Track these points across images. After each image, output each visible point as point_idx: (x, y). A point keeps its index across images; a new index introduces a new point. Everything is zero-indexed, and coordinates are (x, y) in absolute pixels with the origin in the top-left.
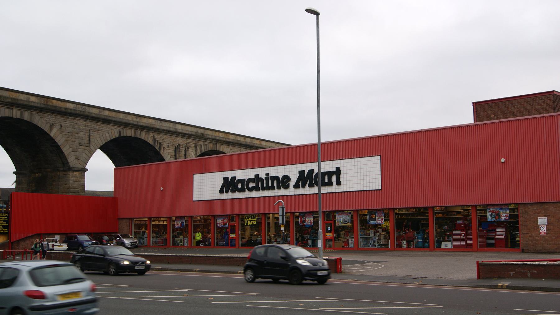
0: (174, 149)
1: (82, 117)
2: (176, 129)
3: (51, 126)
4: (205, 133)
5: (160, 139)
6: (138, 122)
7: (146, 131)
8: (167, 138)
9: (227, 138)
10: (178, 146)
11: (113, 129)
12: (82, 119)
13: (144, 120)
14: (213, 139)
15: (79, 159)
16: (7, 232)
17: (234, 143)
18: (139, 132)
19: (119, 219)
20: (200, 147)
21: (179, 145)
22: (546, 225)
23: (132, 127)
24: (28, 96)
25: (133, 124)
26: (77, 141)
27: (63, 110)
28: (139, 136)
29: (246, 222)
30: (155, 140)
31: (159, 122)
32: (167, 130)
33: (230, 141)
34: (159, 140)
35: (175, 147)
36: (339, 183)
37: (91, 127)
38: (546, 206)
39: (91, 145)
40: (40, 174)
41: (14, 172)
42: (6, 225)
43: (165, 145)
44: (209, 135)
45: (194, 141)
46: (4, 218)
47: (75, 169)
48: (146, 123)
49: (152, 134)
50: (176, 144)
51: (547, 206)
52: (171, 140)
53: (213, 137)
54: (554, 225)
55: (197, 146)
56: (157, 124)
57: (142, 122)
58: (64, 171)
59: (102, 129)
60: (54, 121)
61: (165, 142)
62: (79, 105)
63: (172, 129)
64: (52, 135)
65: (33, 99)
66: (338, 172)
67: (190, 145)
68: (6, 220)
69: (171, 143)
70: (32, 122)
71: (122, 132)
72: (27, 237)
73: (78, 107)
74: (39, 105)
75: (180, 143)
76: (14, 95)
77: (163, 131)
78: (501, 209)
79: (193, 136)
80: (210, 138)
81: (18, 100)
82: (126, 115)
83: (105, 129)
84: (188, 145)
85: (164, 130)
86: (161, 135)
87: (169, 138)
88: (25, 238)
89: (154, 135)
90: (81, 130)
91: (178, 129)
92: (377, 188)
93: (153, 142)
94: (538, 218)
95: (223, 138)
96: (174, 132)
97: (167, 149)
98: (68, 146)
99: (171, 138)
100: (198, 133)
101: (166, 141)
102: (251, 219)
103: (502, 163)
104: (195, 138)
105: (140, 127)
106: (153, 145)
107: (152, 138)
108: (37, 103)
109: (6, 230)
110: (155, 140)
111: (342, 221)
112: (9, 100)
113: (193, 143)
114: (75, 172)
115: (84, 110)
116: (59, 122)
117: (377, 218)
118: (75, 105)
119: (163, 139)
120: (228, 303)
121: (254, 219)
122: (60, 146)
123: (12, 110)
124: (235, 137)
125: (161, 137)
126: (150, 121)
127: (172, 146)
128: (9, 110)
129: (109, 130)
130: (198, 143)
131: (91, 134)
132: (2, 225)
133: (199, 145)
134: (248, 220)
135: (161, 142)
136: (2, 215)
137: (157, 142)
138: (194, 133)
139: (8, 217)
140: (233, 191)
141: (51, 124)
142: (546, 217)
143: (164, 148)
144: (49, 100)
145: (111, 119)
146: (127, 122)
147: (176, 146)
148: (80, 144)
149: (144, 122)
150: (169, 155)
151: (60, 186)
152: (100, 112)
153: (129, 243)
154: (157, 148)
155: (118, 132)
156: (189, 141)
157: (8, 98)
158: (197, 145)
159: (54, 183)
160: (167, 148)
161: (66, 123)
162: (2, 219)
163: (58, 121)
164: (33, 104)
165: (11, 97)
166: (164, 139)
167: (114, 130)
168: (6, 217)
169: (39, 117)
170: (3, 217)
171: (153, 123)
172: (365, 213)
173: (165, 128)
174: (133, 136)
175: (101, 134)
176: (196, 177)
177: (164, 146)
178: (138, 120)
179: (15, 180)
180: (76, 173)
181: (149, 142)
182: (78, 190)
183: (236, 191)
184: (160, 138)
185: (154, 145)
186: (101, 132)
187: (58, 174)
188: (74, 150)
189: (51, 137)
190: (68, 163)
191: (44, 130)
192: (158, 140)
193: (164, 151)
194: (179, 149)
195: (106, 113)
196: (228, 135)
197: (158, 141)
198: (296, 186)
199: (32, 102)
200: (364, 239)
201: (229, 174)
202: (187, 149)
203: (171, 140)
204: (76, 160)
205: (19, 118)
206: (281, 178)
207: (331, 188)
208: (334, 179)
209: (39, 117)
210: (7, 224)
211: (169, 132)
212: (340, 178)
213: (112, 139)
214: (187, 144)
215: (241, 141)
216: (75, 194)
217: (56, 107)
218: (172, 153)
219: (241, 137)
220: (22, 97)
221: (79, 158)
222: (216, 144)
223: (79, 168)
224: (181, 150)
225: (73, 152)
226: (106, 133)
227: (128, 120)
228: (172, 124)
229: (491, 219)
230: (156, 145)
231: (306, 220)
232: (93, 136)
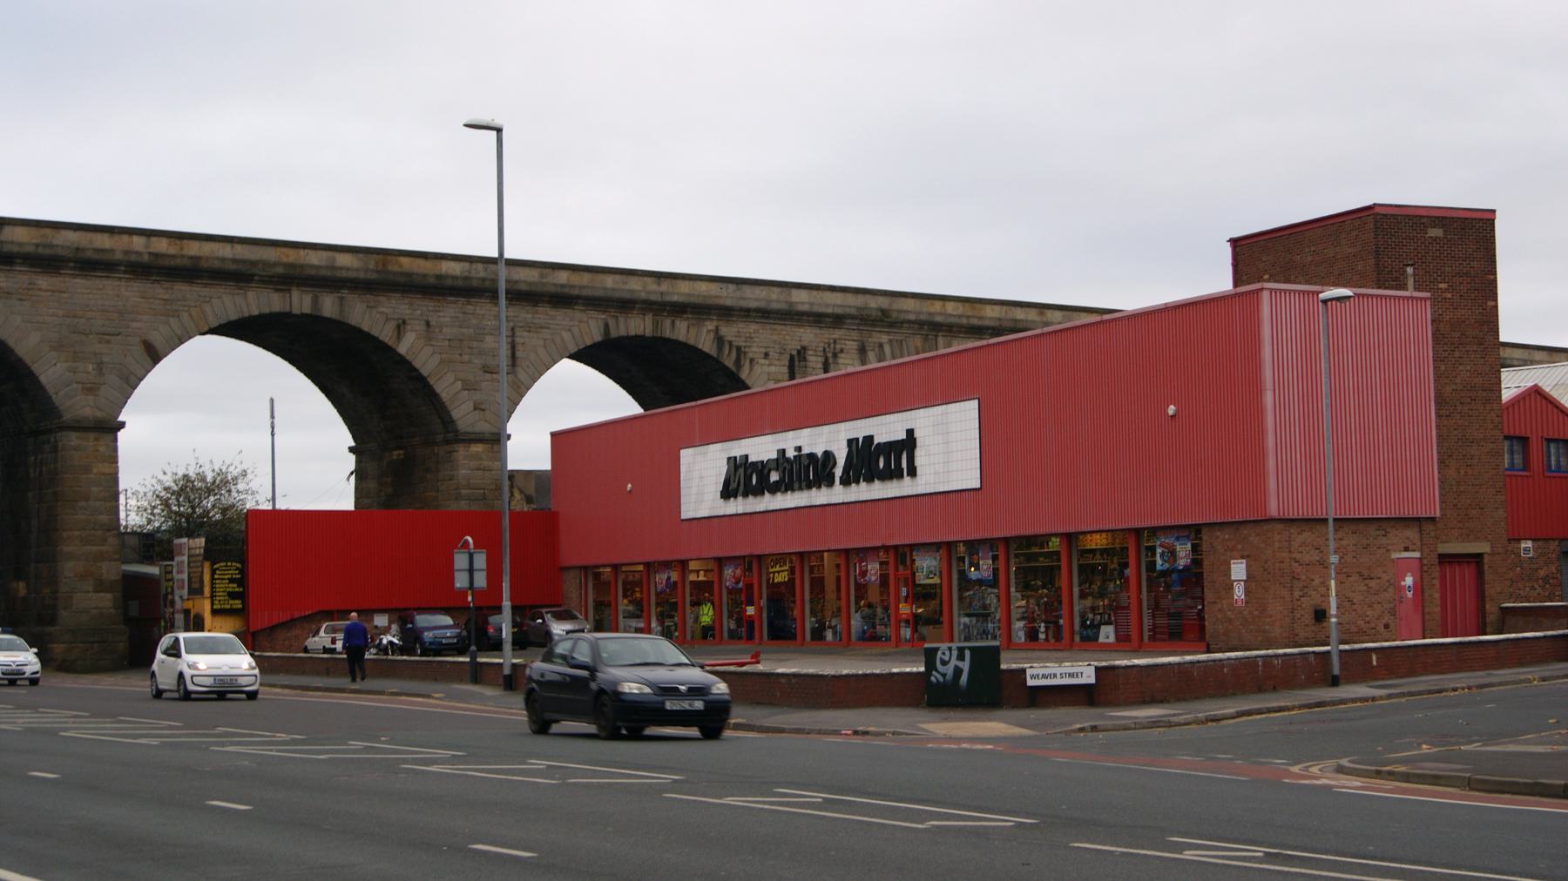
0: (787, 363)
1: (487, 294)
2: (791, 304)
3: (398, 327)
4: (895, 307)
5: (739, 337)
6: (662, 294)
7: (690, 316)
8: (761, 331)
9: (974, 317)
10: (799, 352)
11: (585, 319)
12: (488, 301)
13: (684, 287)
14: (921, 324)
15: (484, 410)
16: (239, 609)
17: (999, 330)
18: (668, 322)
19: (561, 568)
20: (877, 349)
21: (804, 348)
22: (1245, 581)
23: (642, 309)
24: (330, 254)
25: (646, 302)
26: (476, 361)
27: (432, 281)
28: (668, 331)
29: (771, 575)
30: (720, 340)
31: (732, 287)
32: (758, 310)
33: (986, 323)
34: (734, 339)
35: (791, 355)
36: (913, 472)
37: (517, 319)
38: (1245, 531)
39: (519, 370)
40: (402, 452)
41: (349, 448)
42: (237, 590)
43: (755, 351)
44: (907, 312)
45: (855, 335)
46: (232, 574)
47: (472, 437)
48: (689, 295)
49: (710, 325)
50: (793, 346)
51: (1245, 532)
52: (775, 337)
53: (923, 317)
54: (1257, 581)
55: (868, 348)
56: (726, 294)
57: (678, 294)
58: (447, 442)
59: (550, 322)
60: (408, 312)
61: (755, 344)
62: (477, 262)
63: (775, 306)
64: (402, 349)
65: (344, 260)
66: (909, 442)
67: (843, 346)
68: (235, 578)
69: (777, 346)
70: (346, 321)
71: (611, 323)
72: (292, 620)
73: (476, 269)
74: (362, 275)
75: (805, 343)
76: (291, 256)
77: (746, 314)
78: (1178, 539)
79: (848, 321)
80: (910, 322)
81: (302, 266)
82: (624, 277)
83: (559, 322)
84: (835, 349)
85: (748, 310)
86: (741, 325)
87: (770, 332)
88: (287, 622)
89: (717, 328)
90: (486, 332)
91: (797, 303)
92: (974, 487)
93: (715, 345)
94: (1232, 561)
95: (960, 316)
96: (782, 314)
97: (762, 365)
98: (450, 377)
99: (775, 330)
100: (871, 309)
101: (756, 340)
102: (780, 566)
103: (1172, 416)
104: (859, 325)
105: (668, 308)
106: (715, 356)
107: (712, 335)
108: (357, 270)
109: (237, 604)
110: (720, 340)
111: (925, 573)
112: (280, 270)
113: (854, 340)
114: (473, 445)
115: (492, 277)
116: (421, 314)
117: (981, 563)
118: (466, 265)
119: (748, 335)
120: (842, 795)
121: (784, 568)
122: (429, 376)
123: (288, 295)
124: (1006, 312)
125: (741, 330)
126: (703, 287)
127: (781, 353)
128: (281, 294)
129: (571, 324)
130: (870, 340)
131: (518, 340)
132: (228, 590)
133: (875, 343)
134: (774, 570)
135: (740, 344)
136: (226, 566)
137: (727, 347)
138: (853, 311)
139: (241, 571)
141: (401, 321)
142: (1244, 561)
143: (752, 360)
144: (389, 257)
145: (576, 292)
146: (627, 296)
147: (794, 353)
148: (486, 369)
149: (681, 292)
150: (769, 379)
151: (440, 483)
152: (542, 276)
153: (561, 632)
154: (729, 362)
155: (601, 325)
156: (837, 334)
157: (275, 264)
158: (867, 344)
159: (429, 476)
160: (763, 361)
161: (441, 314)
162: (226, 577)
163: (419, 312)
164: (344, 274)
165: (285, 260)
166: (753, 335)
167: (587, 322)
168: (235, 570)
169: (364, 306)
170: (230, 572)
171: (713, 293)
172: (1084, 546)
173: (753, 305)
174: (649, 333)
175: (547, 337)
176: (686, 455)
177: (750, 355)
178: (665, 286)
179: (352, 467)
180: (477, 448)
181: (700, 347)
182: (484, 494)
183: (766, 492)
184: (739, 332)
185: (718, 355)
186: (546, 330)
187: (436, 449)
188: (469, 387)
189: (400, 355)
190: (453, 421)
191: (380, 338)
192: (730, 339)
193: (751, 369)
194: (805, 360)
195: (563, 277)
196: (977, 306)
197: (730, 343)
199: (341, 268)
200: (981, 619)
201: (740, 448)
202: (831, 360)
203: (775, 337)
204: (477, 412)
205: (309, 312)
206: (820, 455)
207: (849, 491)
209: (364, 306)
210: (239, 587)
211: (765, 315)
212: (915, 459)
213: (582, 347)
214: (832, 346)
215: (1027, 321)
216: (475, 507)
217: (409, 275)
218: (783, 373)
219: (1028, 309)
220: (314, 258)
221: (483, 407)
222: (936, 336)
223: (484, 433)
224: (810, 364)
225: (467, 392)
226: (563, 333)
227: (632, 291)
228: (776, 290)
229: (1162, 565)
230: (727, 352)
231: (867, 571)
232: (523, 344)
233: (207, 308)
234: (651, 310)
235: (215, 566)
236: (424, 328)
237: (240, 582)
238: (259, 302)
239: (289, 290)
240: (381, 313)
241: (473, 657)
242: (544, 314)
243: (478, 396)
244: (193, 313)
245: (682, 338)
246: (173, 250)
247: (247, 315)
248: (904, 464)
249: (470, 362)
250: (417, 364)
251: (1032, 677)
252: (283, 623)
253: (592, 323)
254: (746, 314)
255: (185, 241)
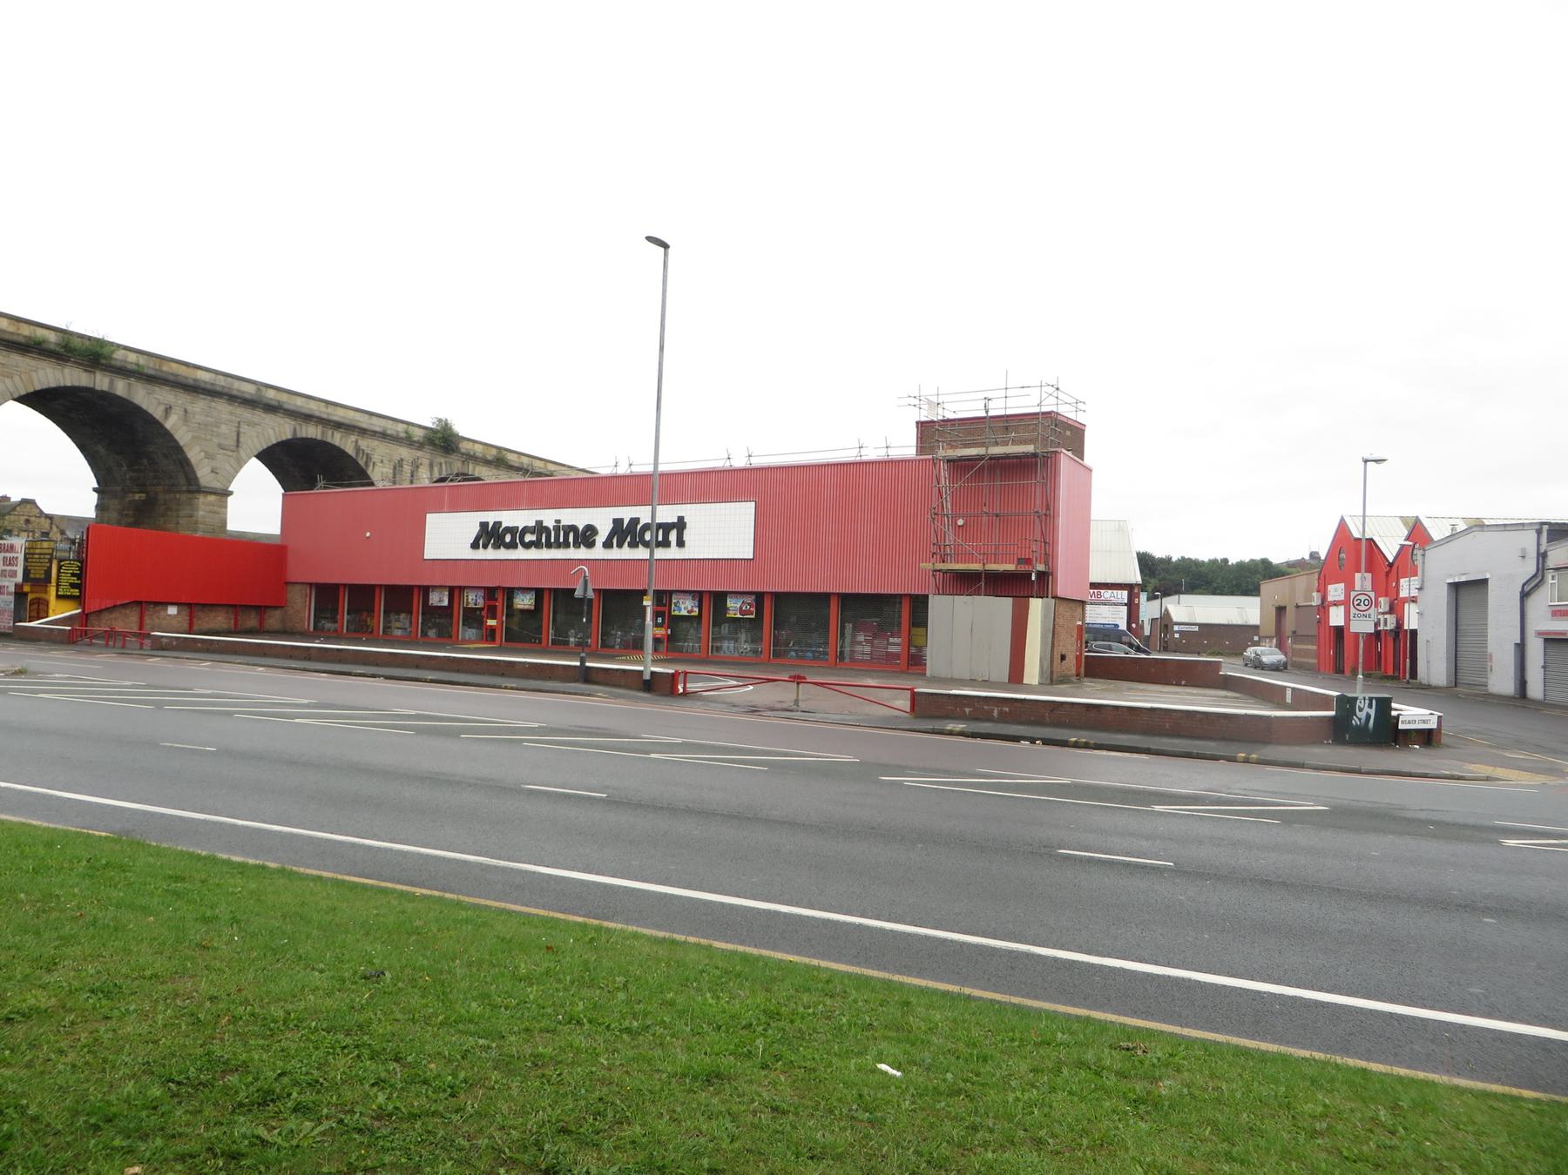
6: (328, 414)
18: (330, 432)
19: (286, 583)
27: (191, 382)
30: (358, 449)
36: (681, 543)
39: (240, 449)
40: (144, 495)
43: (376, 458)
45: (428, 456)
47: (207, 490)
49: (353, 438)
64: (168, 425)
66: (680, 525)
75: (402, 457)
85: (375, 432)
86: (370, 440)
98: (197, 449)
107: (354, 444)
109: (76, 592)
110: (358, 449)
118: (213, 375)
123: (92, 376)
128: (88, 374)
131: (242, 430)
137: (361, 452)
139: (81, 569)
140: (633, 545)
143: (374, 464)
149: (338, 415)
154: (362, 463)
156: (419, 453)
171: (356, 418)
174: (319, 438)
176: (431, 518)
178: (330, 409)
180: (212, 498)
188: (209, 456)
189: (166, 429)
194: (402, 467)
197: (363, 450)
198: (607, 544)
203: (387, 451)
204: (213, 474)
208: (673, 536)
213: (280, 440)
217: (177, 376)
228: (390, 422)
233: (34, 374)
234: (321, 423)
235: (62, 563)
236: (183, 413)
237: (79, 576)
238: (50, 375)
239: (94, 373)
240: (156, 399)
241: (583, 661)
242: (258, 416)
243: (214, 464)
244: (23, 377)
245: (337, 444)
246: (11, 329)
247: (62, 385)
248: (544, 540)
249: (211, 440)
250: (177, 437)
251: (1403, 722)
252: (108, 609)
253: (287, 426)
254: (375, 434)
255: (22, 324)
